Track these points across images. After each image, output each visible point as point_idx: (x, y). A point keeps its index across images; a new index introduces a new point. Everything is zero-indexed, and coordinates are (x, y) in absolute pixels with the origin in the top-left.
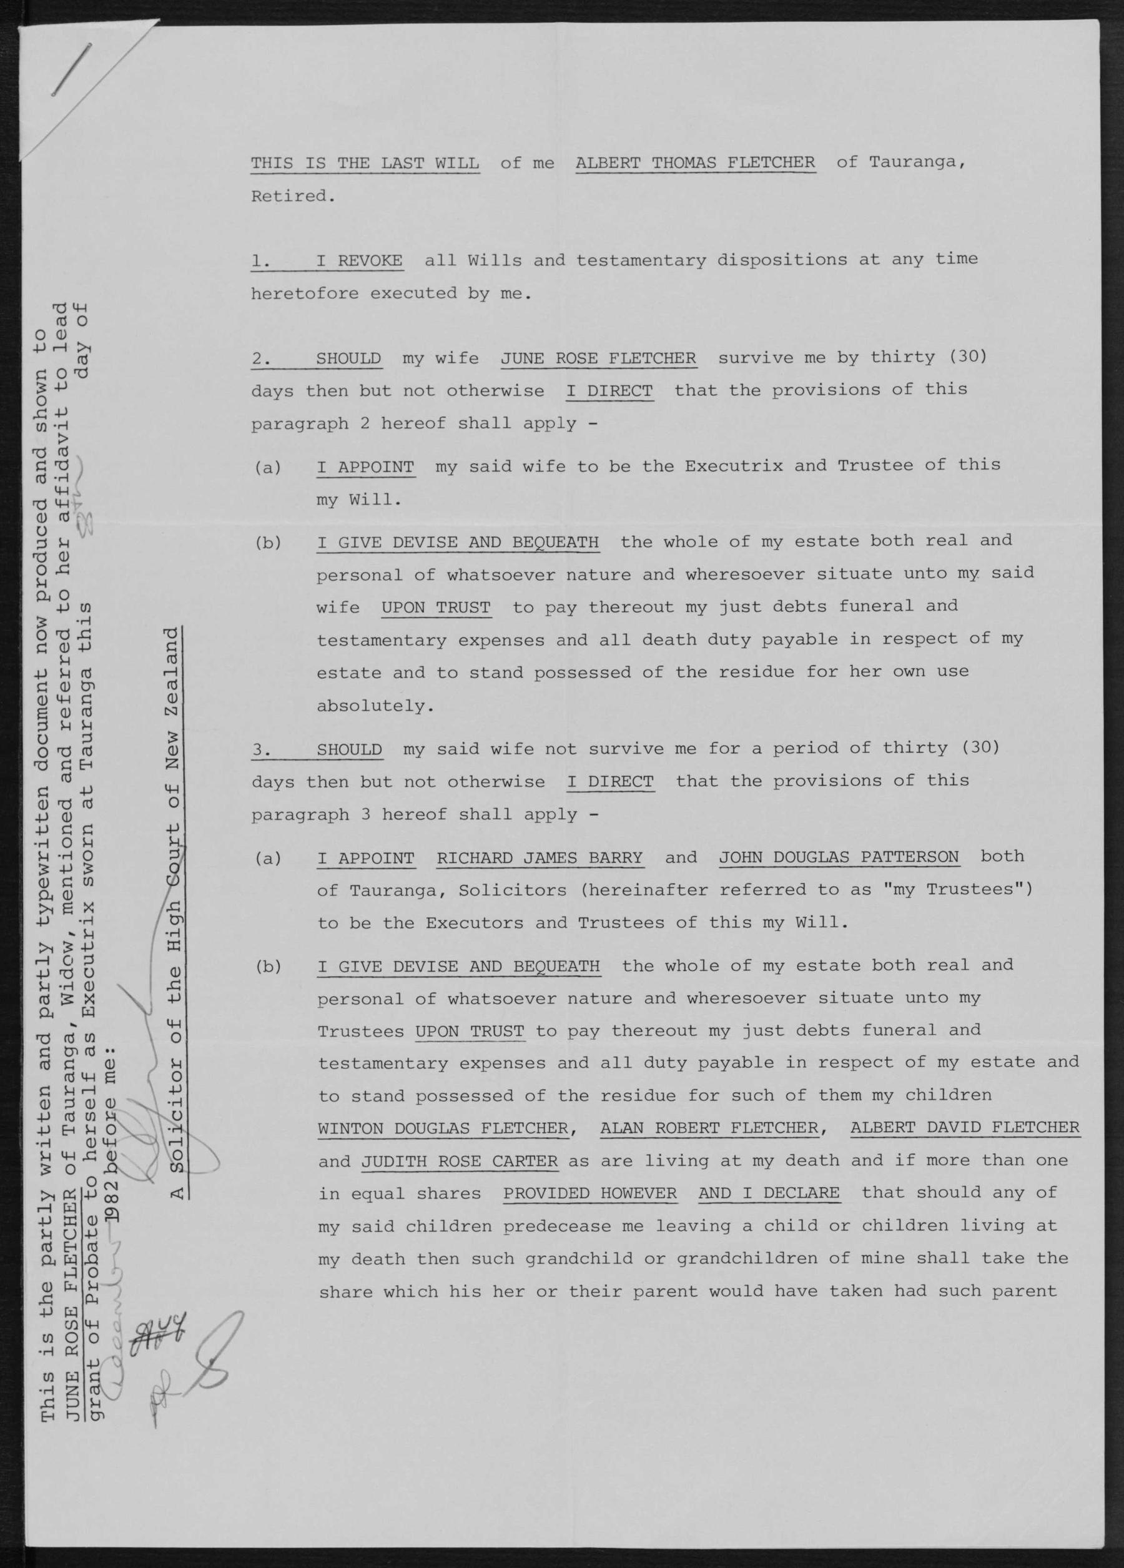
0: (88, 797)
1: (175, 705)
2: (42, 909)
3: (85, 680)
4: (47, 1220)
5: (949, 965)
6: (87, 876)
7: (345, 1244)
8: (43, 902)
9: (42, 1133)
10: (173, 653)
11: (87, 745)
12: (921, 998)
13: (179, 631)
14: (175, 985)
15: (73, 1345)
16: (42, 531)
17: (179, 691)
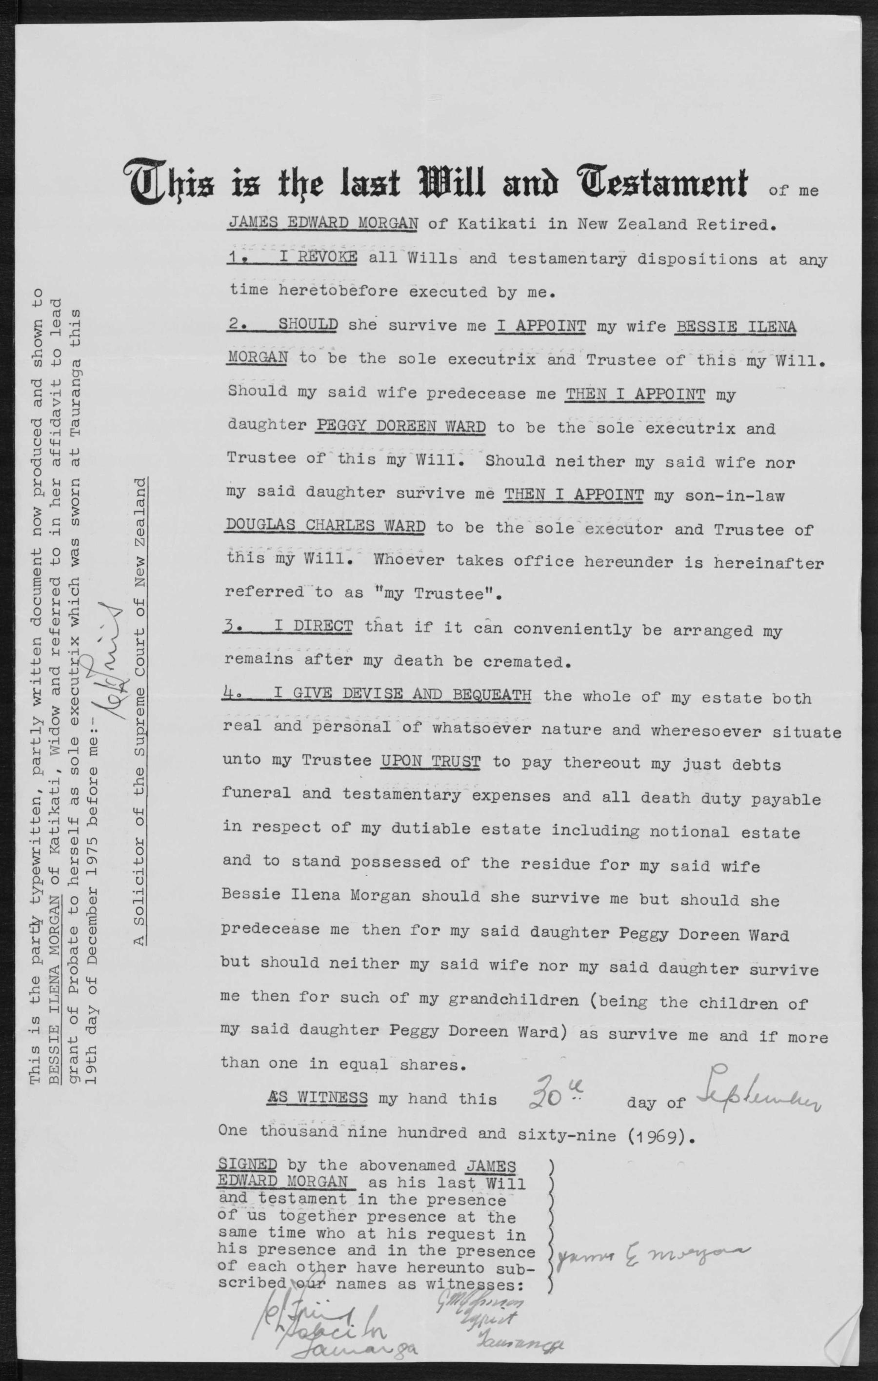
0: (76, 457)
1: (142, 532)
2: (35, 890)
3: (75, 368)
4: (37, 741)
5: (55, 318)
6: (75, 517)
7: (247, 1012)
8: (36, 885)
9: (34, 673)
10: (141, 498)
11: (76, 418)
12: (74, 1050)
13: (146, 481)
14: (140, 781)
15: (55, 926)
16: (38, 442)
17: (145, 527)
